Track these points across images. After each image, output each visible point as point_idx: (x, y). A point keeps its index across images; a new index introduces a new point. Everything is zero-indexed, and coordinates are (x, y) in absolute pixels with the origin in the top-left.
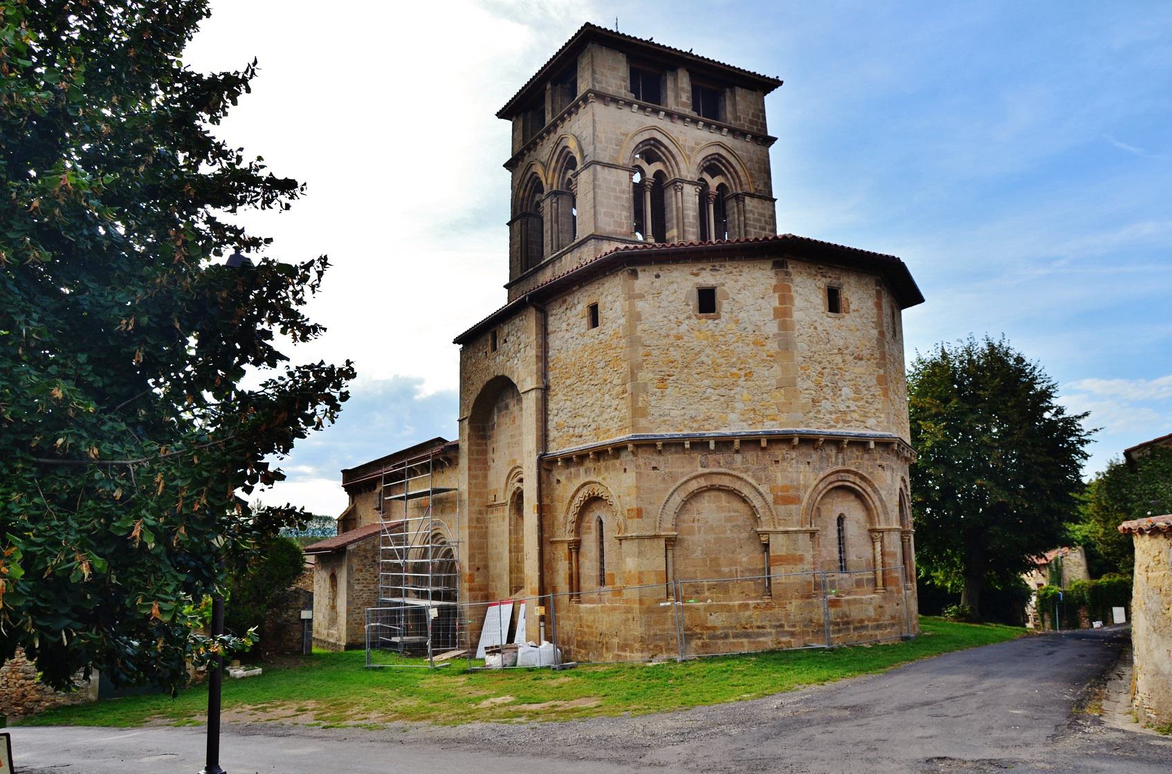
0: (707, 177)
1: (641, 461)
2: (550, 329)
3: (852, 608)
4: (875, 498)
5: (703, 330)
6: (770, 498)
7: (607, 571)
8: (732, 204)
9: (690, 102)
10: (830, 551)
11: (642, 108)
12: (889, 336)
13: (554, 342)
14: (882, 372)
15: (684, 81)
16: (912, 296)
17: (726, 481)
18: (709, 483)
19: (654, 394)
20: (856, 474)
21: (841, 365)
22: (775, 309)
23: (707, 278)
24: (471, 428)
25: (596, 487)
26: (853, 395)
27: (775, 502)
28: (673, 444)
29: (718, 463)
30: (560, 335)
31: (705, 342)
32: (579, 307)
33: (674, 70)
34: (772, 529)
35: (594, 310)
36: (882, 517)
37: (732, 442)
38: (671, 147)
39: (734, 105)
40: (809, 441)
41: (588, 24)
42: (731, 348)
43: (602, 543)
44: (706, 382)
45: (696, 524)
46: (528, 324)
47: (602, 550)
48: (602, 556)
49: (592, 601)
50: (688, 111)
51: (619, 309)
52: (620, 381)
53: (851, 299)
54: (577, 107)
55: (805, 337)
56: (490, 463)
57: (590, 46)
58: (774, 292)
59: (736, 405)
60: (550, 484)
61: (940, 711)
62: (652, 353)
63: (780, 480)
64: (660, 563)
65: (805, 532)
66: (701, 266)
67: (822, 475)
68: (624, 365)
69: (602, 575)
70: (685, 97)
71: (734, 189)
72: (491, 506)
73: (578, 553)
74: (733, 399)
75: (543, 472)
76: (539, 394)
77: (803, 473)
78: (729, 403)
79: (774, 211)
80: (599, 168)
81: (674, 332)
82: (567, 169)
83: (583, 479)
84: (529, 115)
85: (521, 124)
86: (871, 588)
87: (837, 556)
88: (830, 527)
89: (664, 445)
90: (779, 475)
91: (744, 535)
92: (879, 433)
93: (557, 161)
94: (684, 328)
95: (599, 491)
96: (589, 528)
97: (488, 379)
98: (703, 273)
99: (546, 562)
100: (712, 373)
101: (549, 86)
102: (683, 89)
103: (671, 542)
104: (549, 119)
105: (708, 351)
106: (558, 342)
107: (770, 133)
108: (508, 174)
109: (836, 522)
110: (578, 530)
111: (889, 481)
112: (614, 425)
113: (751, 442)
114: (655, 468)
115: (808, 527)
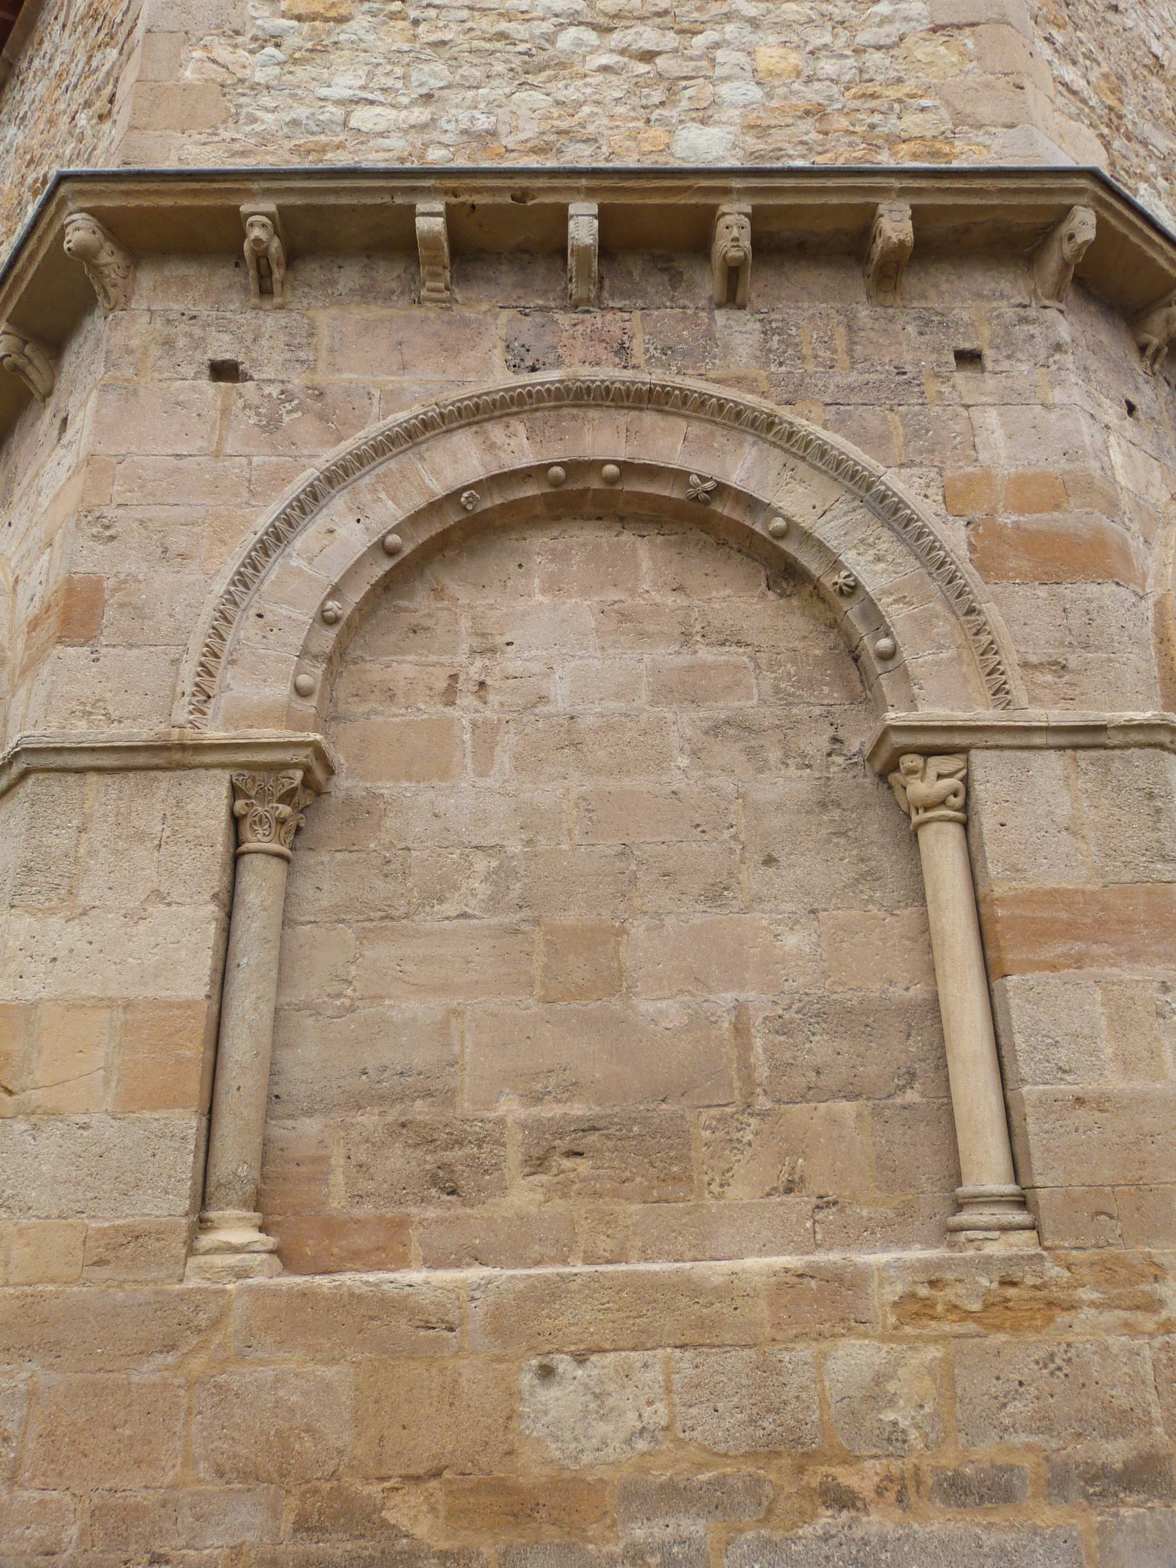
17: (668, 444)
64: (173, 951)
88: (559, 446)
91: (786, 785)
114: (224, 371)
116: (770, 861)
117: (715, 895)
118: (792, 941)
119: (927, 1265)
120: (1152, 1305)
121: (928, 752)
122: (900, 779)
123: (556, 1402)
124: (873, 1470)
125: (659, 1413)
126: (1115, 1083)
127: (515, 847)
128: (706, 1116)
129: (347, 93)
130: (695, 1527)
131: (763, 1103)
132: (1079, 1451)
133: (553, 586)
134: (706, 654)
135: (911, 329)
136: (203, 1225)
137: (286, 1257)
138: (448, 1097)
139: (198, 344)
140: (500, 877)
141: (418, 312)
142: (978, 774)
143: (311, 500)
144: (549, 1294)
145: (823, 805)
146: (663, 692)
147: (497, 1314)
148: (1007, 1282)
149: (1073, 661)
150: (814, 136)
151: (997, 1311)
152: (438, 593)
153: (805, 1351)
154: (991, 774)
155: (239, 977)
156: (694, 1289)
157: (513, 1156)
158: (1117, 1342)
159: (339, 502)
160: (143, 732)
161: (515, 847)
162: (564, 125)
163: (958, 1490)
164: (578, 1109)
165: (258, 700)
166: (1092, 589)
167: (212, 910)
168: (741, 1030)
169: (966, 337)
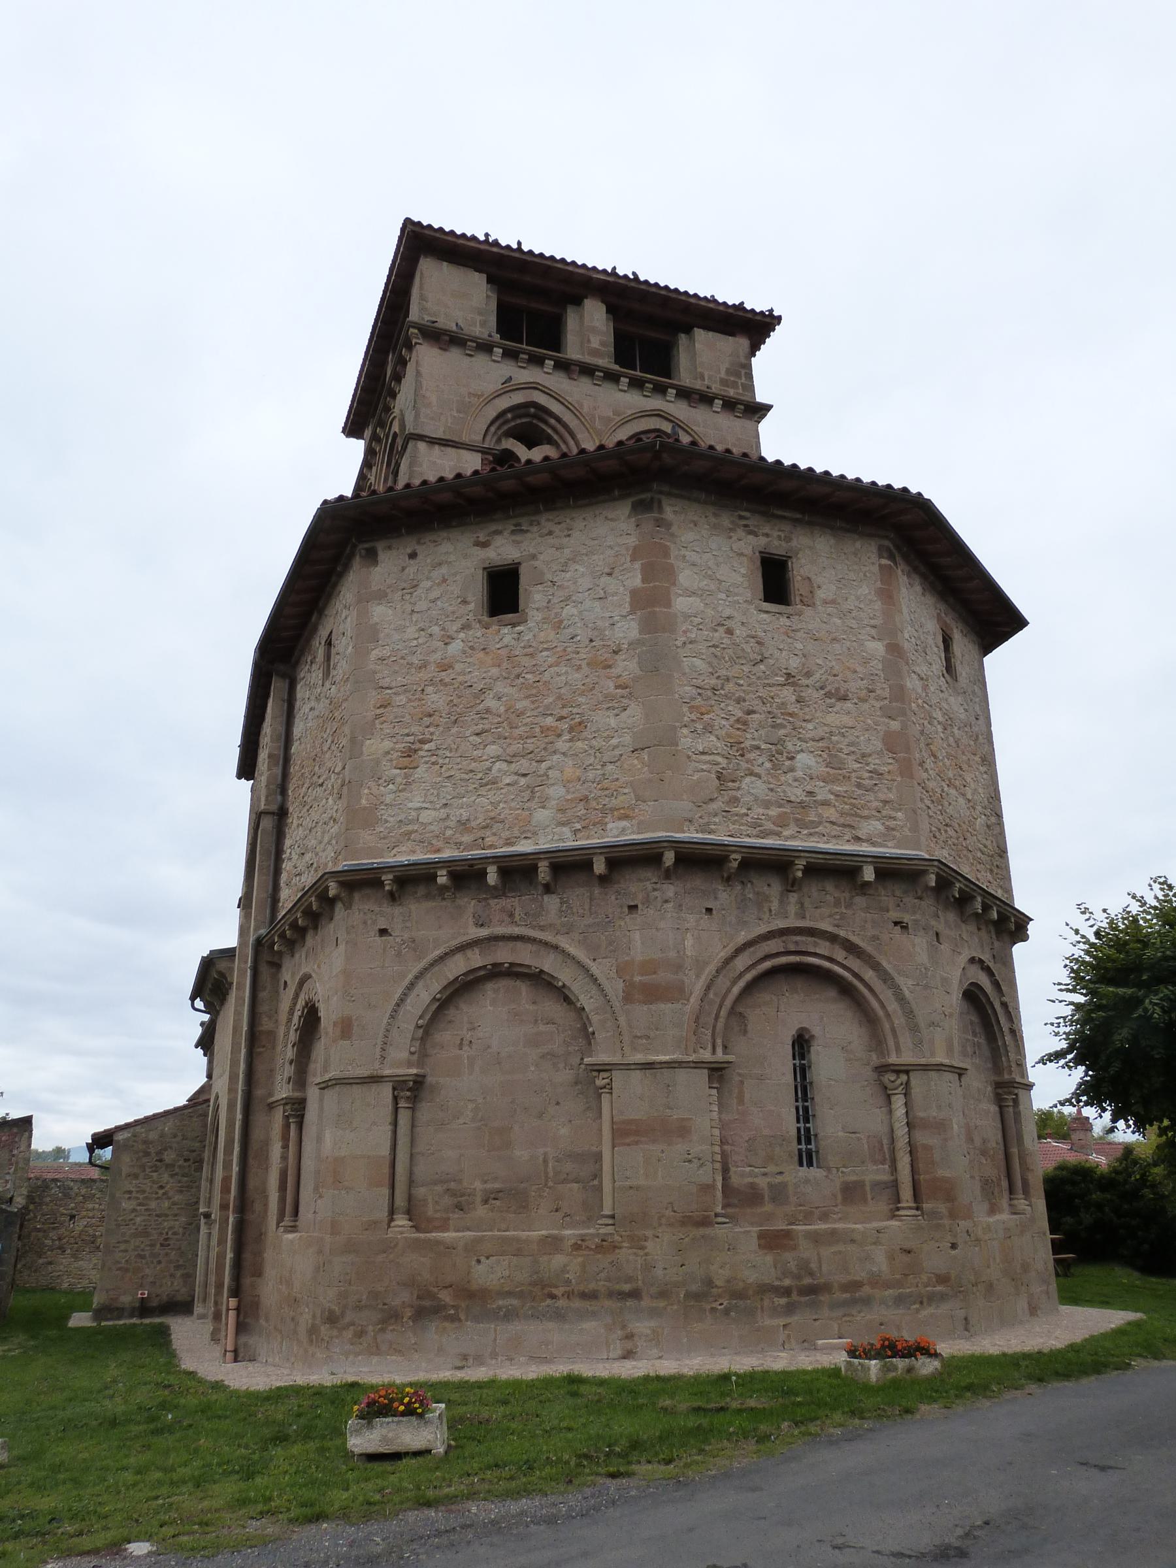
3: (827, 1252)
4: (886, 995)
6: (615, 988)
10: (770, 1107)
14: (895, 725)
16: (991, 617)
17: (524, 956)
19: (392, 781)
20: (833, 938)
21: (792, 708)
22: (634, 593)
23: (504, 549)
26: (823, 769)
27: (628, 998)
28: (412, 881)
29: (507, 915)
31: (495, 671)
33: (578, 301)
34: (616, 1059)
36: (905, 1039)
37: (535, 868)
38: (567, 417)
40: (699, 861)
44: (493, 750)
45: (466, 1052)
53: (818, 580)
58: (633, 560)
65: (698, 1065)
66: (494, 527)
67: (743, 937)
77: (691, 935)
78: (534, 792)
80: (422, 446)
81: (437, 656)
86: (883, 1206)
87: (790, 1125)
90: (637, 936)
91: (564, 1076)
92: (890, 850)
94: (456, 647)
98: (499, 541)
99: (254, 1146)
100: (504, 730)
105: (500, 687)
107: (761, 397)
111: (923, 957)
113: (569, 867)
114: (383, 932)
115: (706, 1055)
116: (558, 1103)
117: (540, 1116)
118: (564, 1131)
119: (581, 1235)
120: (642, 1248)
121: (599, 1071)
122: (594, 1081)
123: (481, 1268)
124: (562, 1289)
125: (507, 1273)
126: (642, 1182)
127: (480, 1100)
128: (534, 1188)
129: (419, 805)
130: (515, 1302)
131: (550, 1184)
132: (617, 1287)
134: (542, 1028)
135: (613, 897)
136: (391, 1220)
137: (417, 1228)
138: (460, 1181)
139: (374, 922)
141: (444, 903)
142: (913, 1082)
143: (412, 986)
144: (479, 1240)
145: (576, 1083)
148: (603, 1240)
149: (652, 1034)
150: (583, 812)
151: (599, 1249)
152: (457, 1008)
153: (546, 1258)
155: (399, 1147)
156: (517, 1240)
157: (478, 1199)
158: (631, 1258)
159: (421, 984)
160: (366, 1073)
161: (480, 1100)
162: (492, 814)
163: (584, 1296)
164: (497, 1186)
165: (399, 1062)
166: (663, 1006)
167: (390, 1127)
168: (545, 1161)
169: (633, 900)
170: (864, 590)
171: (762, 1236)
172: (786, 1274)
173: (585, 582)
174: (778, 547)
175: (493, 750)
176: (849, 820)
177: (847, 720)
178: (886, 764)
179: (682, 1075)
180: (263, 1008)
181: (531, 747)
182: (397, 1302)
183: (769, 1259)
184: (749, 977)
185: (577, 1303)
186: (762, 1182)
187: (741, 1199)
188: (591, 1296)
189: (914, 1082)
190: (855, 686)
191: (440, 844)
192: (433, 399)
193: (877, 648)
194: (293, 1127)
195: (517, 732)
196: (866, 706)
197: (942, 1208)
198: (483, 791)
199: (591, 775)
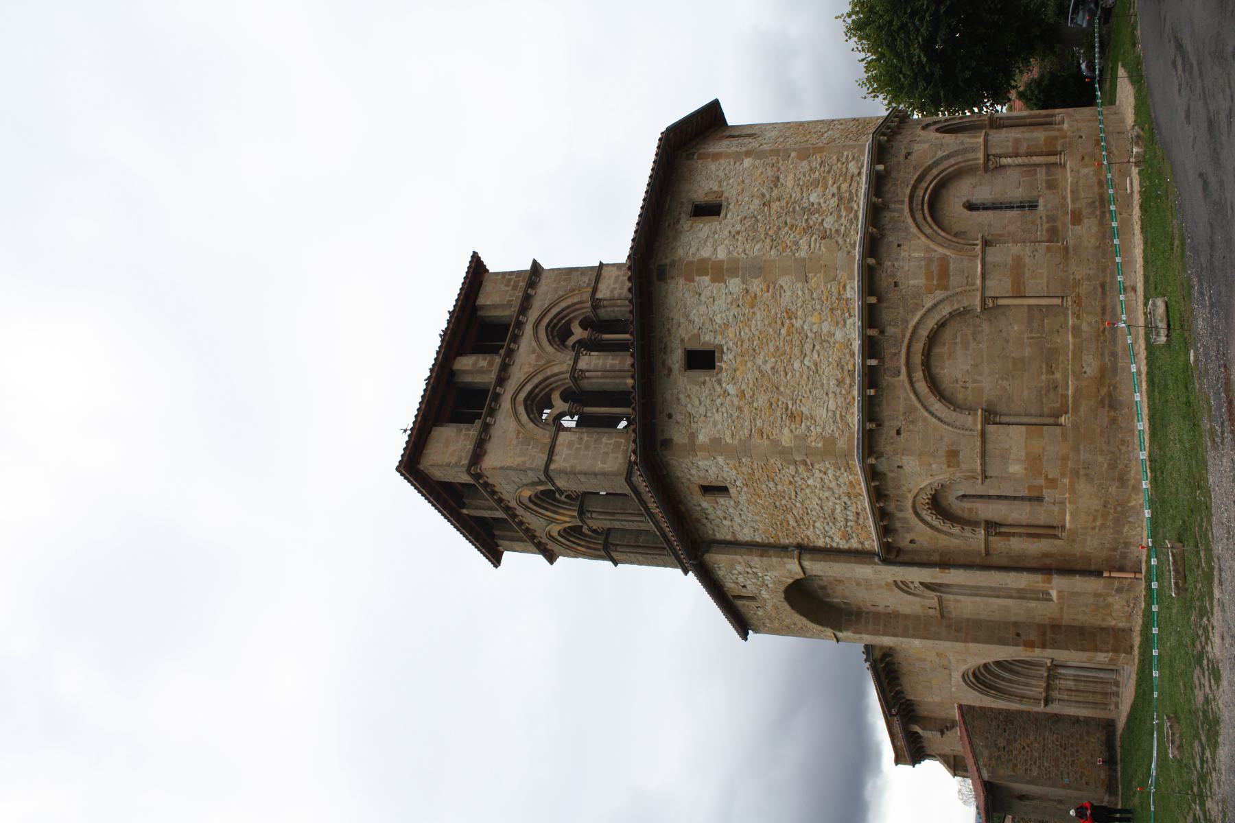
0: (571, 341)
1: (889, 449)
2: (729, 537)
3: (1082, 195)
4: (946, 164)
5: (734, 365)
6: (940, 294)
7: (1025, 493)
8: (603, 313)
9: (488, 357)
11: (492, 412)
12: (754, 144)
13: (746, 535)
14: (793, 154)
15: (465, 363)
16: (694, 137)
17: (919, 347)
18: (920, 368)
19: (808, 428)
21: (784, 203)
22: (713, 280)
23: (676, 359)
24: (847, 630)
25: (920, 500)
26: (820, 189)
27: (946, 288)
28: (871, 410)
30: (737, 528)
31: (749, 364)
32: (705, 505)
33: (453, 373)
34: (979, 294)
35: (708, 490)
36: (970, 156)
37: (870, 337)
38: (536, 381)
39: (495, 306)
40: (873, 246)
41: (398, 469)
42: (757, 333)
43: (990, 497)
44: (796, 365)
45: (970, 385)
46: (721, 562)
47: (999, 497)
48: (1006, 498)
49: (1063, 513)
50: (498, 360)
51: (707, 463)
52: (792, 468)
53: (707, 189)
54: (486, 485)
55: (747, 246)
56: (889, 610)
57: (421, 467)
58: (693, 281)
59: (825, 330)
60: (915, 552)
61: (1223, 116)
62: (774, 391)
63: (918, 281)
64: (1017, 433)
65: (984, 252)
67: (914, 230)
68: (772, 461)
69: (1030, 499)
70: (482, 361)
71: (587, 308)
72: (942, 615)
73: (1001, 525)
74: (818, 334)
75: (901, 558)
76: (806, 556)
77: (913, 253)
78: (824, 340)
79: (614, 265)
80: (552, 467)
81: (735, 400)
82: (555, 499)
83: (909, 513)
84: (497, 533)
85: (507, 543)
86: (1059, 171)
89: (871, 420)
90: (912, 282)
91: (985, 327)
92: (866, 159)
93: (546, 509)
94: (731, 389)
95: (925, 498)
96: (971, 510)
97: (788, 608)
98: (669, 362)
100: (785, 358)
101: (465, 511)
102: (474, 364)
103: (991, 415)
104: (499, 514)
105: (759, 361)
106: (746, 531)
107: (527, 266)
108: (561, 560)
109: (974, 213)
110: (974, 524)
111: (926, 146)
112: (845, 477)
113: (871, 317)
114: (898, 432)
115: (978, 248)
117: (1007, 341)
122: (990, 308)
123: (1089, 371)
126: (1045, 280)
133: (942, 368)
134: (958, 340)
140: (1003, 379)
144: (1073, 371)
146: (967, 348)
147: (1077, 380)
151: (1079, 304)
154: (990, 293)
163: (1103, 314)
165: (974, 421)
170: (713, 167)
171: (1073, 224)
172: (1093, 213)
173: (702, 309)
174: (688, 208)
175: (796, 365)
176: (849, 177)
177: (791, 177)
178: (816, 161)
179: (989, 259)
180: (925, 559)
181: (798, 342)
182: (1106, 420)
183: (1086, 221)
184: (935, 228)
185: (1108, 317)
186: (1046, 226)
187: (1054, 234)
188: (1104, 308)
189: (993, 152)
190: (770, 173)
191: (850, 397)
192: (519, 460)
193: (747, 162)
194: (1002, 530)
195: (788, 351)
196: (782, 168)
197: (1060, 141)
198: (821, 371)
199: (818, 307)
